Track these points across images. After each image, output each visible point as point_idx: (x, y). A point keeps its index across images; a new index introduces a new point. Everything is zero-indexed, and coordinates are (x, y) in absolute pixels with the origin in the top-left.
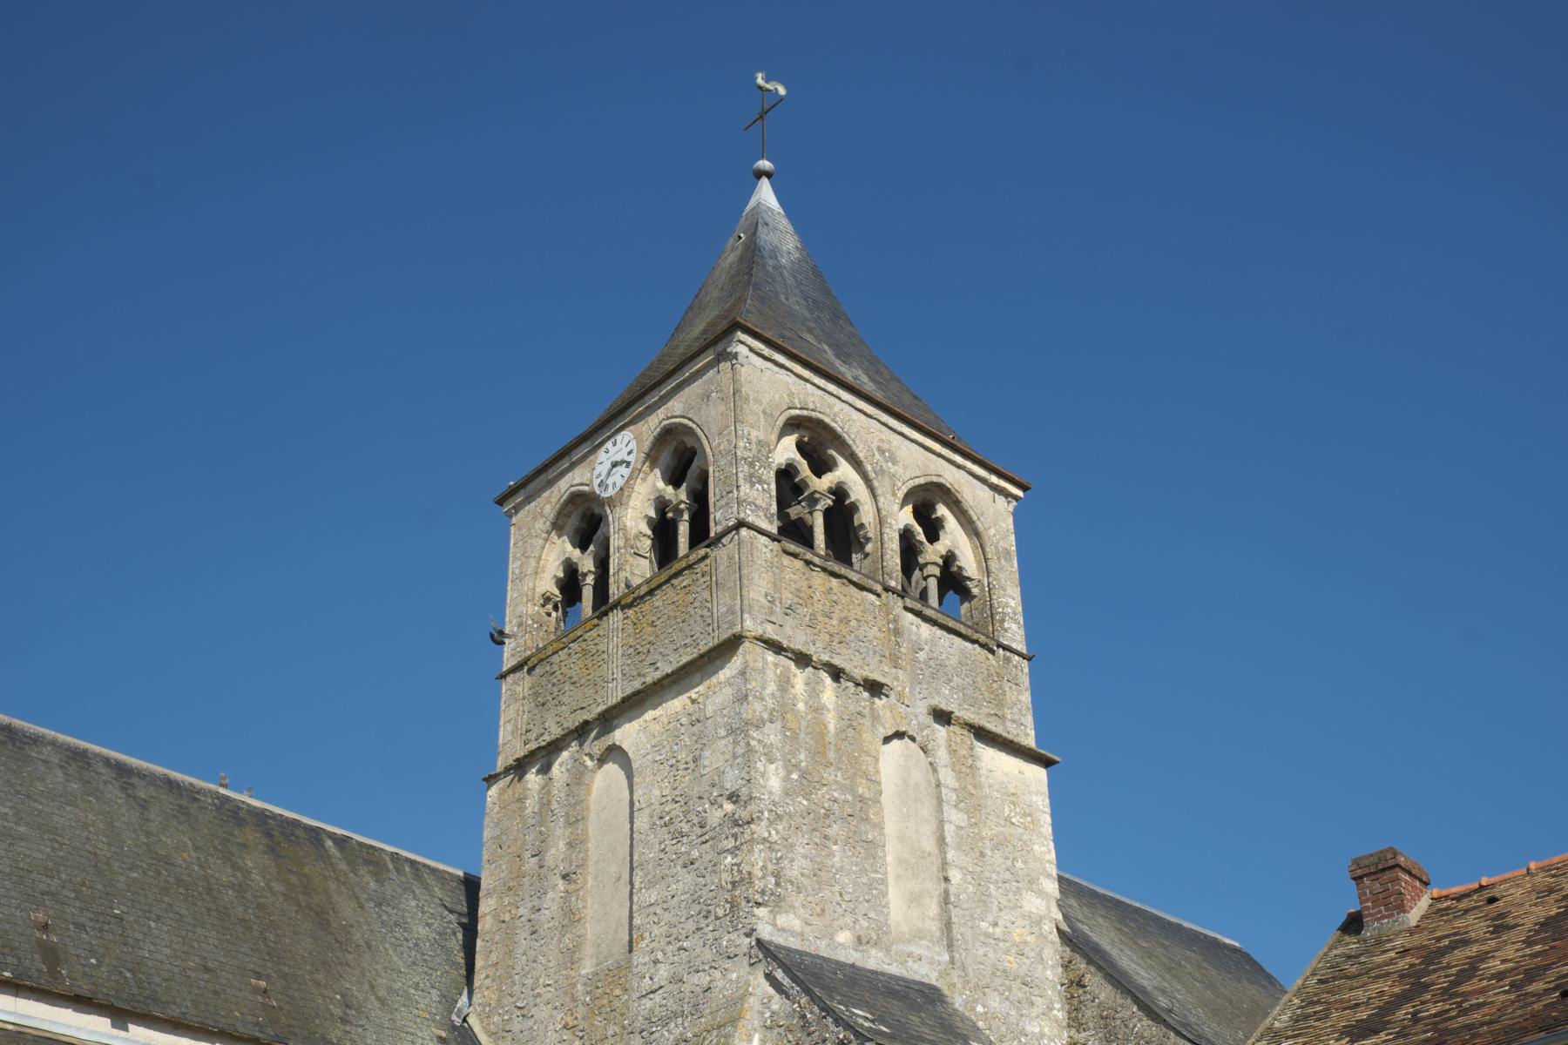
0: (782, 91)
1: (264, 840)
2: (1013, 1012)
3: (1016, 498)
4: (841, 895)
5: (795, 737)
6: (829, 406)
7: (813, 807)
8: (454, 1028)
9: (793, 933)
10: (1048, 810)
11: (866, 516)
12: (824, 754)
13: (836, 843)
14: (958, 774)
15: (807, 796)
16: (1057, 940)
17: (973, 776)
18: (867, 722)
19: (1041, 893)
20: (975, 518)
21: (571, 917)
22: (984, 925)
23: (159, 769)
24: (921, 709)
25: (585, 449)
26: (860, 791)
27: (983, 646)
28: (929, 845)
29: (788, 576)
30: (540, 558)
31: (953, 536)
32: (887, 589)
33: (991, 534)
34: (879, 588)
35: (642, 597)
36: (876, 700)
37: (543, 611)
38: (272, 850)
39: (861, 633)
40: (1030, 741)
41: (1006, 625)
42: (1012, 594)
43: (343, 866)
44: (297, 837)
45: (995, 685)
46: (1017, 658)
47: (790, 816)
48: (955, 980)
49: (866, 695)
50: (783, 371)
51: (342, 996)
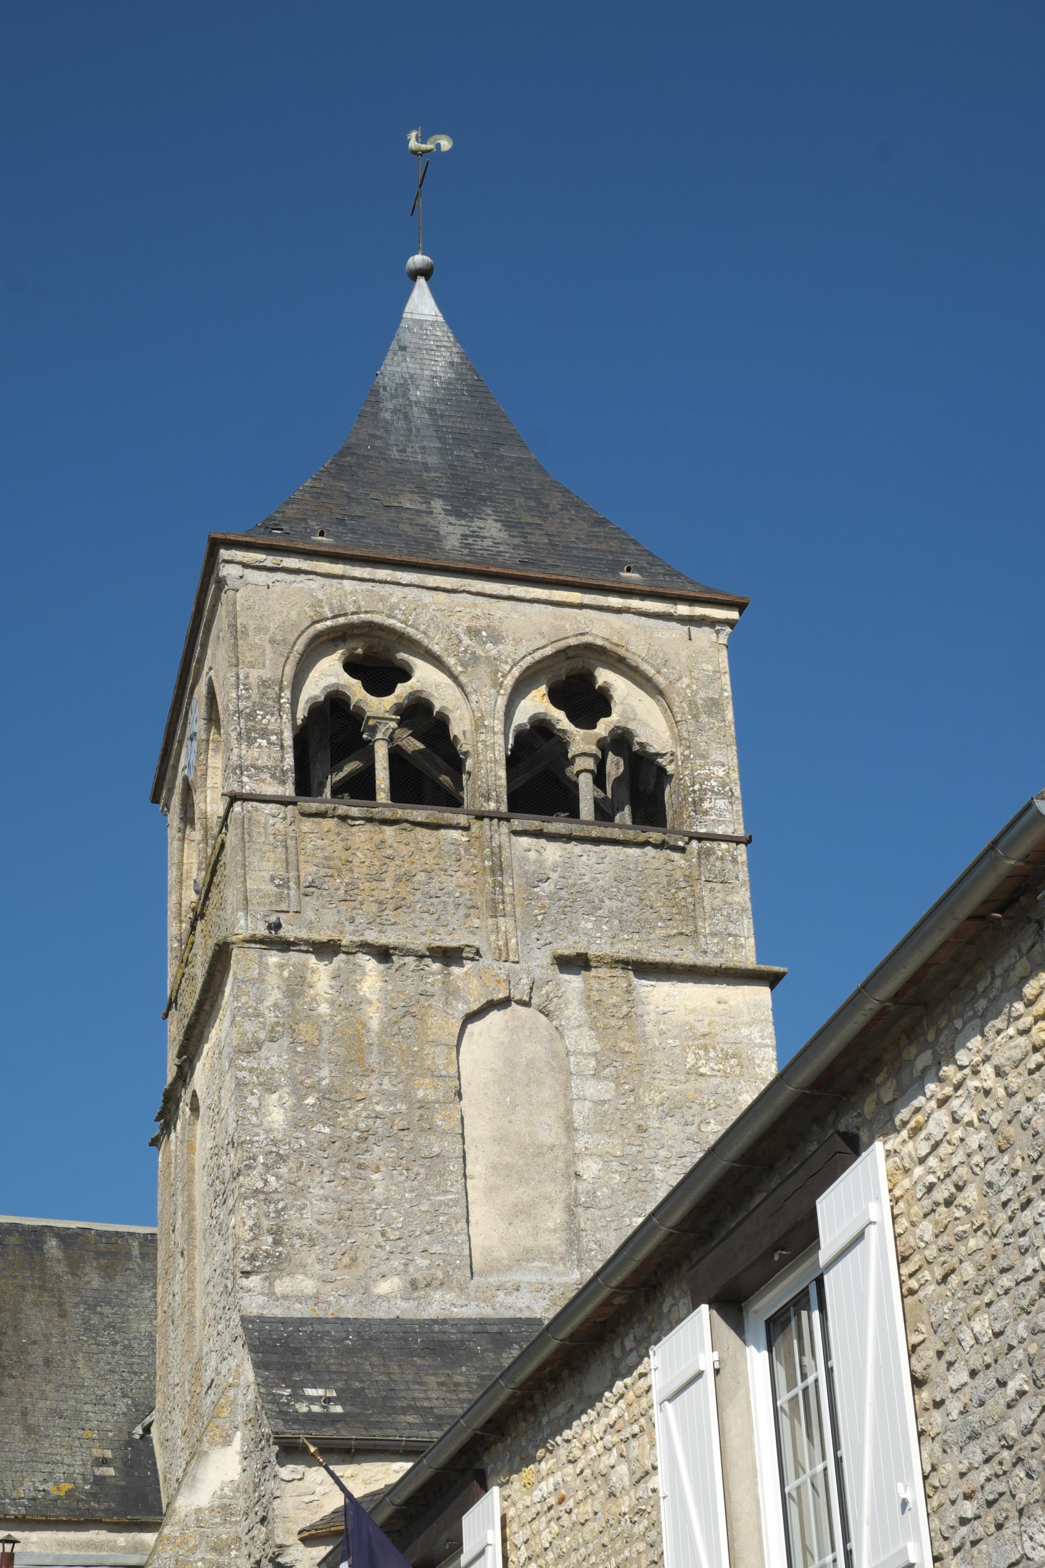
0: (446, 144)
3: (731, 623)
4: (383, 1234)
5: (312, 1050)
7: (340, 1133)
8: (131, 1442)
9: (299, 1299)
10: (771, 1041)
11: (459, 727)
13: (377, 1170)
14: (601, 1031)
17: (630, 1028)
20: (651, 672)
24: (540, 961)
26: (421, 1094)
27: (661, 846)
28: (550, 1134)
32: (480, 817)
36: (455, 970)
39: (433, 887)
41: (706, 805)
43: (60, 1269)
45: (681, 894)
46: (724, 845)
47: (301, 1151)
49: (436, 966)
50: (303, 577)
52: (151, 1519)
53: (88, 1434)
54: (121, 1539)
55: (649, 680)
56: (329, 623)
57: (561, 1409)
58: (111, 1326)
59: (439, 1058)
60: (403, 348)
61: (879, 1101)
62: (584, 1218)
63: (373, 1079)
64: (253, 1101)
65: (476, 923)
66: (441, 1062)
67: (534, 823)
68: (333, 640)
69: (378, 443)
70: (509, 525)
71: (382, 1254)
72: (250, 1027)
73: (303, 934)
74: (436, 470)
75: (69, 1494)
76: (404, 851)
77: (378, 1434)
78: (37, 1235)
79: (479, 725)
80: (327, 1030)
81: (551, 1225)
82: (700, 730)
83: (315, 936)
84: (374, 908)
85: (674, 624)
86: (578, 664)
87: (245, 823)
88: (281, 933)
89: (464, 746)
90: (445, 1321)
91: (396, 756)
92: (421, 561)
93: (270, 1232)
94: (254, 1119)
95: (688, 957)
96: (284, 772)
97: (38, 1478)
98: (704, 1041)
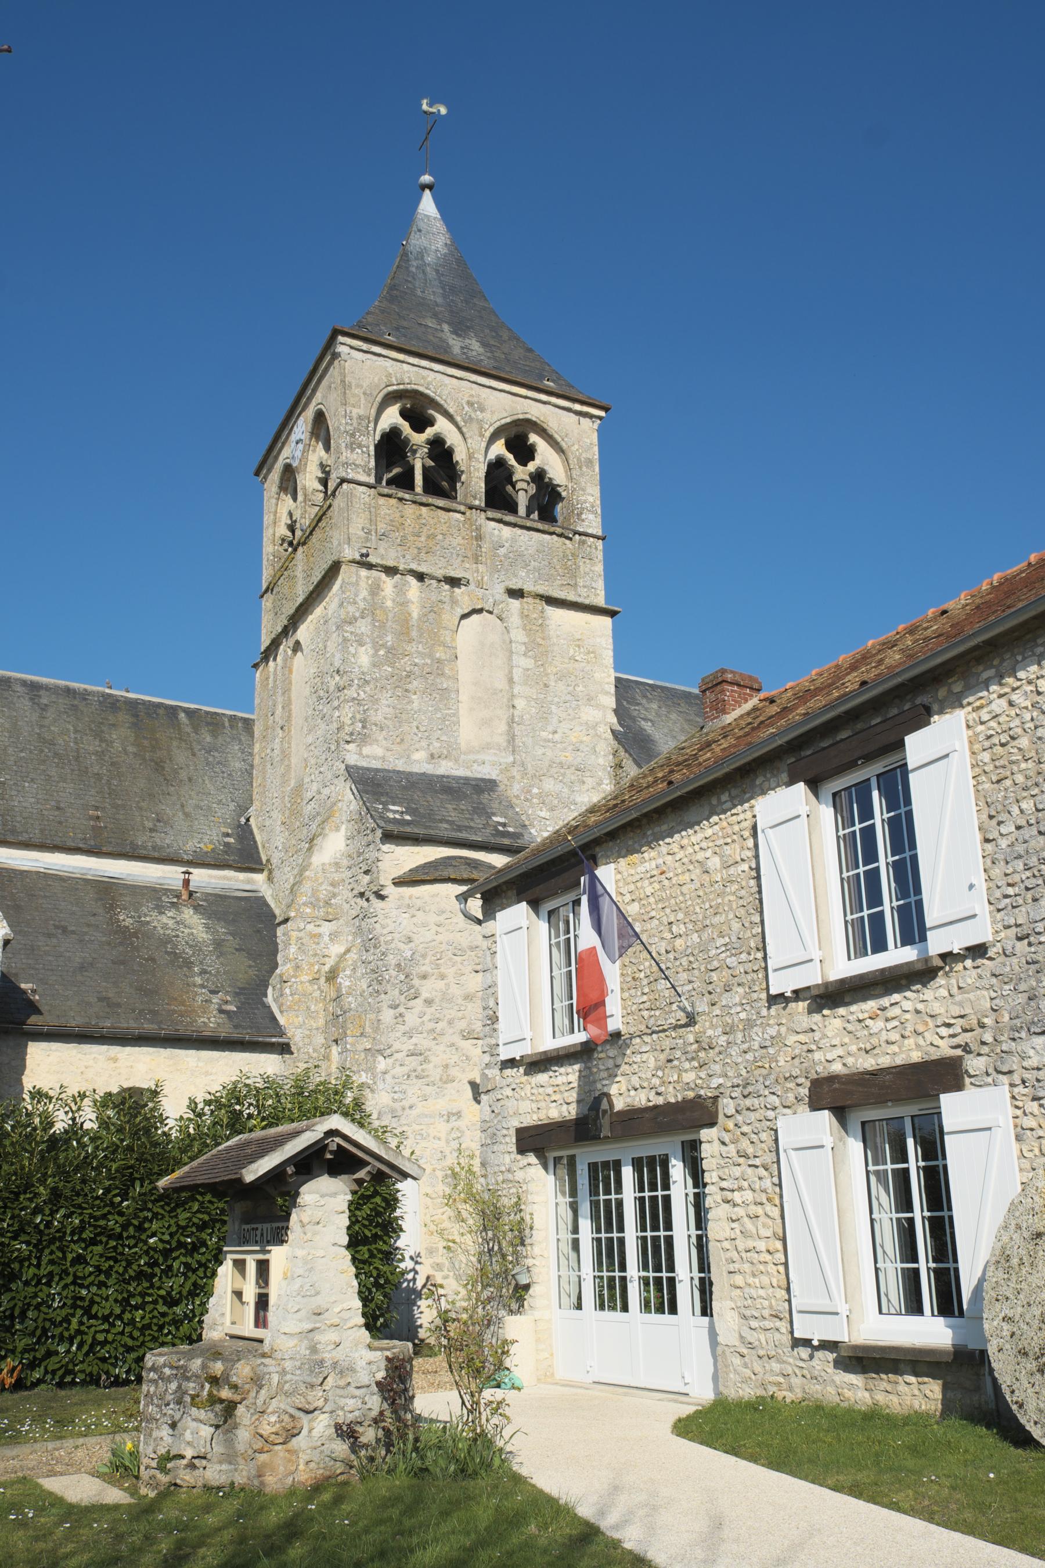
0: (443, 111)
1: (131, 720)
2: (566, 790)
3: (600, 418)
4: (418, 728)
5: (383, 626)
6: (423, 378)
7: (396, 672)
8: (239, 826)
9: (375, 758)
10: (611, 647)
11: (460, 456)
12: (408, 634)
13: (415, 693)
14: (528, 632)
15: (392, 665)
16: (611, 737)
17: (542, 632)
18: (447, 607)
19: (598, 707)
20: (559, 439)
21: (285, 755)
22: (544, 734)
23: (62, 683)
24: (499, 591)
25: (286, 432)
26: (438, 655)
27: (560, 535)
28: (501, 684)
29: (384, 511)
30: (276, 512)
31: (545, 456)
32: (471, 508)
33: (574, 450)
34: (462, 508)
35: (308, 537)
36: (456, 590)
37: (281, 549)
38: (136, 726)
39: (446, 544)
40: (600, 601)
41: (583, 516)
42: (591, 492)
43: (189, 729)
44: (157, 715)
45: (569, 563)
46: (592, 539)
47: (376, 680)
48: (515, 774)
49: (447, 587)
50: (382, 359)
51: (157, 815)
52: (258, 867)
53: (216, 819)
54: (242, 876)
55: (557, 443)
56: (395, 388)
57: (664, 827)
58: (218, 763)
59: (446, 636)
60: (420, 231)
61: (950, 691)
62: (517, 729)
63: (414, 644)
64: (352, 650)
65: (467, 566)
66: (448, 639)
67: (498, 515)
68: (394, 397)
69: (410, 285)
70: (484, 344)
71: (416, 738)
72: (351, 609)
73: (379, 561)
74: (442, 306)
75: (213, 850)
76: (432, 522)
77: (432, 832)
78: (173, 711)
79: (471, 457)
80: (391, 615)
81: (500, 731)
82: (582, 475)
83: (384, 562)
84: (416, 551)
85: (572, 414)
86: (521, 429)
87: (350, 496)
88: (368, 559)
89: (462, 467)
90: (448, 777)
91: (425, 469)
92: (442, 358)
93: (360, 721)
94: (353, 660)
95: (572, 597)
96: (370, 470)
97: (195, 841)
98: (579, 643)
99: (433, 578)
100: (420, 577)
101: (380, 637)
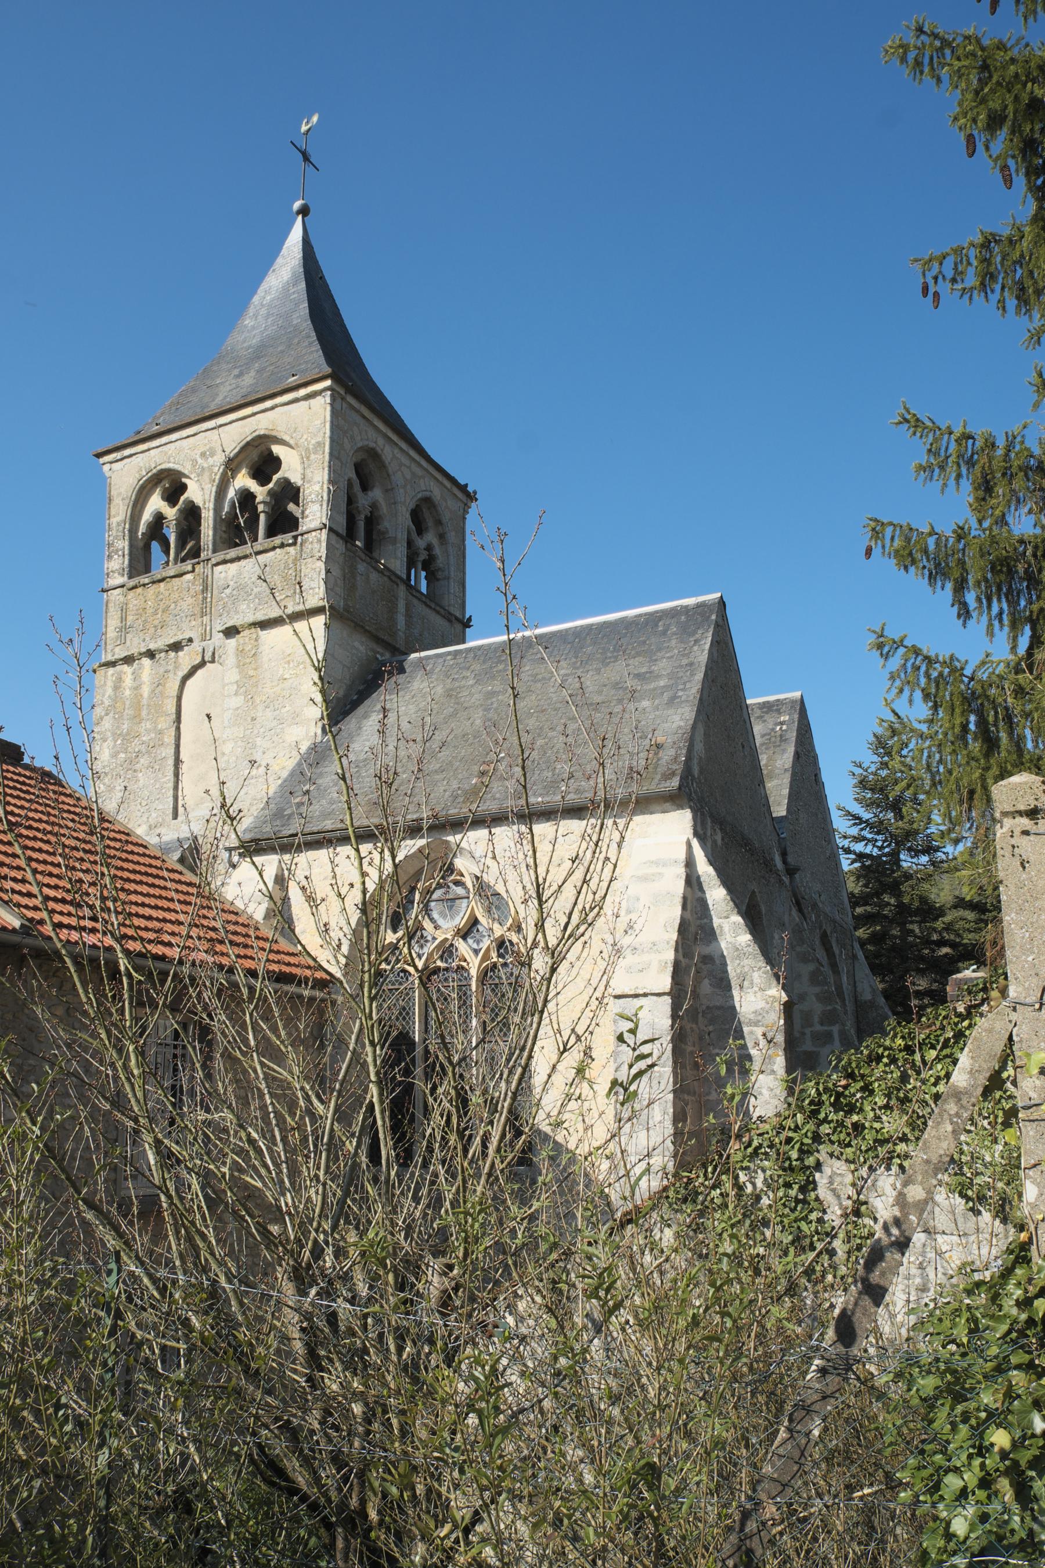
36: (180, 654)
85: (302, 403)
86: (262, 448)
99: (161, 651)
100: (151, 654)
101: (118, 727)
